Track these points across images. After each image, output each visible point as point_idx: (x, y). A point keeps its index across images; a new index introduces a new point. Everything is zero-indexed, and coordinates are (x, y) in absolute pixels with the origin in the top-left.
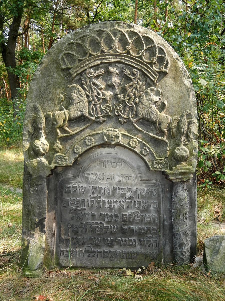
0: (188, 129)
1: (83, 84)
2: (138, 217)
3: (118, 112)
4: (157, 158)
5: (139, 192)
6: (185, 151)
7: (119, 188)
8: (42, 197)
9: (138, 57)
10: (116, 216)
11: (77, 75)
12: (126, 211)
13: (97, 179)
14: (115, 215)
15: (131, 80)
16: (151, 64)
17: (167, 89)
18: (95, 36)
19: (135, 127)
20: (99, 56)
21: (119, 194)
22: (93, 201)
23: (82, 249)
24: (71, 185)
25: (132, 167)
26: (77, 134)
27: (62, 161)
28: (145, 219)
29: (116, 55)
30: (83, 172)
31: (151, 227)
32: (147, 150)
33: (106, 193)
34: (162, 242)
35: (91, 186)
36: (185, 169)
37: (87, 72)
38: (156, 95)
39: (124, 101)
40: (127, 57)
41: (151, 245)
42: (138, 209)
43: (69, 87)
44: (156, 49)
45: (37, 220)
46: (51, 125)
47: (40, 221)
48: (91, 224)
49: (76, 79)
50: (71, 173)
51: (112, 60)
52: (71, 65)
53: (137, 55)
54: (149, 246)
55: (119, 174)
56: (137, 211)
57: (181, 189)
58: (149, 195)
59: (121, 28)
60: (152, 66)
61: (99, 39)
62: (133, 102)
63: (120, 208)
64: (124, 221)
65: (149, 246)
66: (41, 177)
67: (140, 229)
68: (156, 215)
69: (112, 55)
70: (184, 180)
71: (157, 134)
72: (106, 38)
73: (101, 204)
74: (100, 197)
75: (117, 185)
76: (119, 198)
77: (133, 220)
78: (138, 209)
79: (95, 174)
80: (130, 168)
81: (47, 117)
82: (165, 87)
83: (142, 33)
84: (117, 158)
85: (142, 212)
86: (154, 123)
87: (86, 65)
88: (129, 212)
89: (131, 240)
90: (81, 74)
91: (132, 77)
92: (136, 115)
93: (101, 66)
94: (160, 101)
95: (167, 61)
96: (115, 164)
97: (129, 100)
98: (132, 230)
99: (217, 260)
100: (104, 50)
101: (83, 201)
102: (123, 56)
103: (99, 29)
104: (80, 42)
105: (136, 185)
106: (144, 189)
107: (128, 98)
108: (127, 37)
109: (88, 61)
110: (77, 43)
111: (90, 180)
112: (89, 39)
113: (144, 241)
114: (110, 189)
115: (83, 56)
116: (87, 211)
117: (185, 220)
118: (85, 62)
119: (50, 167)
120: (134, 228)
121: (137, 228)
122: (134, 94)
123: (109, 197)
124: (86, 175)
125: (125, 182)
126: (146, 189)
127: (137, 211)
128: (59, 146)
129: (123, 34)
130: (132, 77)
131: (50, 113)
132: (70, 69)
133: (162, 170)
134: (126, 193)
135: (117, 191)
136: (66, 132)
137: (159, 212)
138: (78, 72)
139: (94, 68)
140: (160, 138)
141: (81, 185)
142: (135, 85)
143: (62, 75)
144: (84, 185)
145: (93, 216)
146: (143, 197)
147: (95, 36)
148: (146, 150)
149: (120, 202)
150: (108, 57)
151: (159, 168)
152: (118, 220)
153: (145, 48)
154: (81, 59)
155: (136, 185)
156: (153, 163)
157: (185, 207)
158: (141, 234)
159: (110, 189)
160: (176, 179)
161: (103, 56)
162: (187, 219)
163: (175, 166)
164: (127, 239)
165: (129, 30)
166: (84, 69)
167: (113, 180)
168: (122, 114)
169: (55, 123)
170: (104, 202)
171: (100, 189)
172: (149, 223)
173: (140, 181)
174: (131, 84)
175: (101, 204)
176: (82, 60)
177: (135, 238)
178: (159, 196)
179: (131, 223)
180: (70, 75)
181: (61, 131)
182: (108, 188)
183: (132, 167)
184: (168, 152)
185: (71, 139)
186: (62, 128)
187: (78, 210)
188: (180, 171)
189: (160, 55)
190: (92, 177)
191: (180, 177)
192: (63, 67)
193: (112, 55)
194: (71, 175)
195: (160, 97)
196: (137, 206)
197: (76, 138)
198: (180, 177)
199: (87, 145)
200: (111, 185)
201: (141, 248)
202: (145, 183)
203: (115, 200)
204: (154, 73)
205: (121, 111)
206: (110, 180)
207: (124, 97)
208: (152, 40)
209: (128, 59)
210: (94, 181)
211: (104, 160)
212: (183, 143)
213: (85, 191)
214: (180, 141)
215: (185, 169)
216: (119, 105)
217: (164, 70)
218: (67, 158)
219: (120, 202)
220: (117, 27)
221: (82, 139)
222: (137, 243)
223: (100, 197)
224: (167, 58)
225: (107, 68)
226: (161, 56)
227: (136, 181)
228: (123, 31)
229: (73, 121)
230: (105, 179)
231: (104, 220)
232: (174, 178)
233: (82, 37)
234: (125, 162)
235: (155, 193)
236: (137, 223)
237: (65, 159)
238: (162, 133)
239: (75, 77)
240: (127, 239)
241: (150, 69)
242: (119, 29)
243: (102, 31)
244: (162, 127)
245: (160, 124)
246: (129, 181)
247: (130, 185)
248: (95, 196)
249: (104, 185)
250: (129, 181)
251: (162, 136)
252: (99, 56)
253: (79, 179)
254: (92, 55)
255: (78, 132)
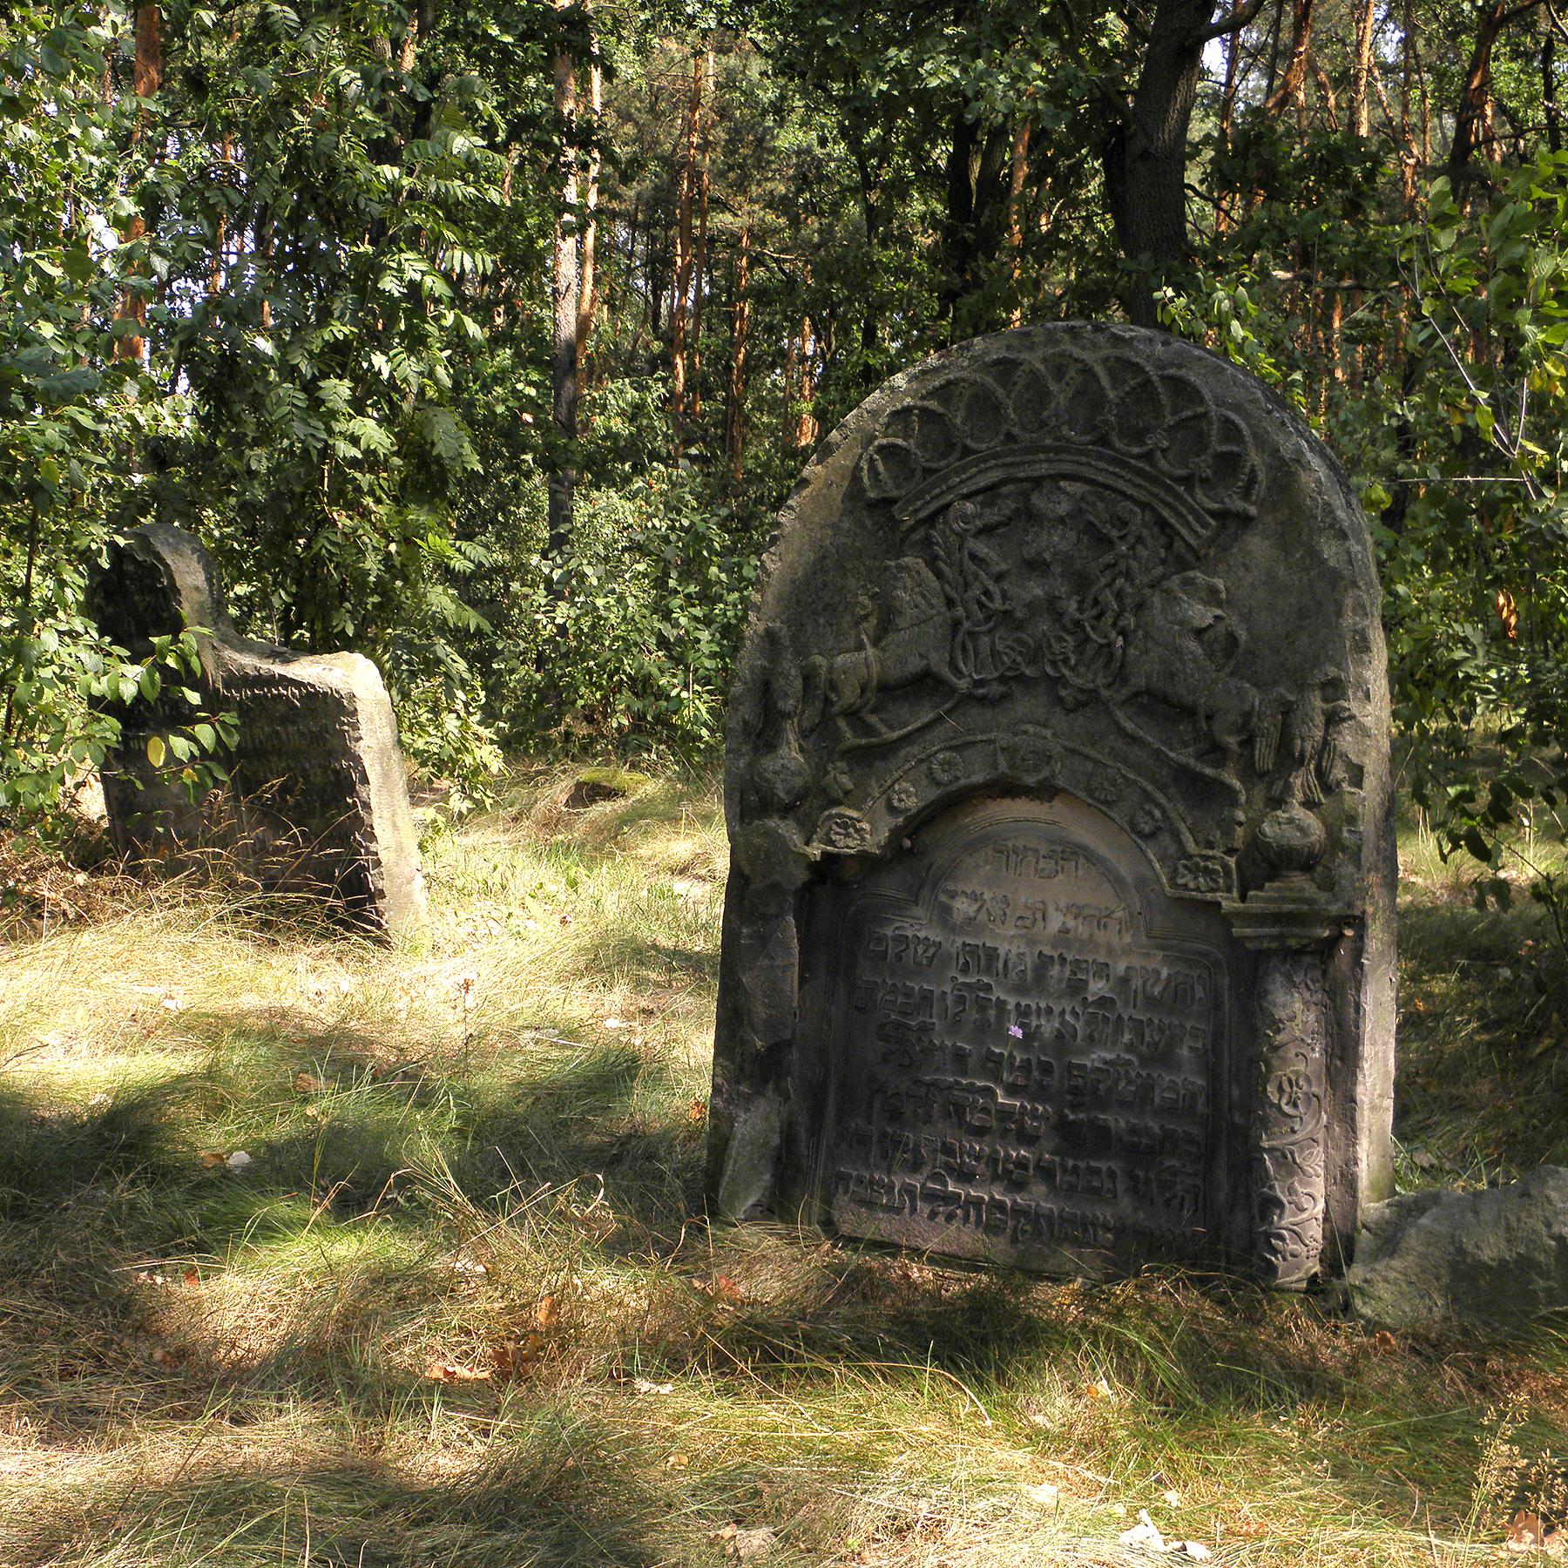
0: (1325, 742)
1: (936, 557)
2: (1129, 1083)
3: (1054, 664)
4: (1191, 846)
5: (1136, 983)
6: (1301, 829)
7: (1063, 959)
8: (779, 962)
9: (1138, 457)
10: (1046, 1069)
11: (920, 523)
12: (1083, 1052)
13: (983, 916)
14: (1039, 1062)
15: (1111, 544)
16: (1187, 481)
17: (1249, 579)
18: (989, 380)
19: (1117, 724)
20: (997, 456)
21: (1060, 980)
22: (961, 1000)
23: (916, 1181)
24: (889, 932)
25: (1117, 881)
26: (907, 739)
27: (847, 835)
28: (1157, 1091)
29: (1057, 450)
30: (935, 884)
31: (1178, 1127)
32: (1157, 814)
33: (1013, 975)
34: (1222, 1196)
35: (959, 943)
36: (1294, 901)
37: (951, 513)
38: (1206, 603)
39: (1078, 623)
40: (1100, 457)
41: (1176, 1202)
42: (1130, 1048)
43: (887, 569)
44: (1210, 423)
45: (759, 1044)
46: (819, 704)
47: (770, 1049)
48: (950, 1087)
49: (916, 537)
50: (890, 886)
51: (1043, 469)
52: (898, 487)
53: (1136, 450)
54: (1168, 1202)
55: (1062, 904)
56: (1127, 1057)
57: (1279, 978)
58: (1176, 996)
59: (1083, 348)
60: (1190, 490)
61: (1000, 392)
62: (1114, 625)
63: (1060, 1036)
64: (1075, 1091)
65: (1168, 1202)
66: (775, 887)
67: (1133, 1130)
68: (1200, 1082)
69: (1046, 449)
70: (1293, 943)
71: (1199, 757)
72: (1028, 386)
73: (992, 1012)
74: (988, 988)
75: (1054, 947)
76: (1060, 997)
77: (1110, 1090)
78: (1130, 1048)
79: (975, 897)
80: (1106, 886)
81: (808, 677)
82: (1241, 572)
83: (1160, 366)
84: (1061, 842)
85: (1145, 1061)
86: (1189, 712)
87: (950, 489)
88: (1096, 1057)
89: (1098, 1172)
90: (931, 520)
91: (1115, 533)
92: (1120, 676)
93: (1005, 490)
94: (1221, 628)
95: (1253, 470)
96: (1051, 865)
97: (1098, 617)
98: (1104, 1131)
99: (1386, 1280)
100: (1016, 431)
101: (927, 997)
102: (1081, 453)
103: (1003, 354)
104: (933, 404)
105: (1127, 951)
106: (1158, 973)
107: (1094, 612)
108: (1105, 381)
109: (957, 472)
110: (924, 410)
111: (958, 917)
112: (967, 394)
113: (1148, 1181)
114: (1029, 960)
115: (944, 456)
116: (942, 1038)
117: (1286, 1109)
118: (945, 478)
119: (805, 856)
120: (1112, 1124)
121: (1122, 1124)
122: (1119, 596)
123: (1021, 989)
124: (943, 898)
125: (1086, 936)
126: (1164, 973)
127: (1127, 1057)
128: (844, 779)
129: (1087, 371)
130: (1115, 533)
131: (818, 659)
132: (894, 501)
133: (1209, 896)
134: (1086, 982)
135: (1055, 971)
136: (869, 730)
137: (1212, 1071)
138: (922, 515)
139: (980, 498)
140: (1208, 771)
141: (922, 935)
142: (1122, 566)
143: (868, 523)
144: (935, 935)
145: (960, 1057)
146: (1151, 1003)
147: (989, 380)
148: (1150, 814)
149: (1063, 1013)
150: (1029, 458)
151: (1198, 889)
152: (1054, 1082)
153: (1170, 420)
154: (934, 465)
155: (1127, 951)
156: (1175, 870)
157: (1291, 1054)
158: (1139, 1152)
159: (1029, 960)
160: (1259, 938)
161: (1013, 452)
162: (1295, 1106)
163: (1261, 888)
164: (1082, 1165)
165: (1116, 352)
166: (942, 502)
167: (1040, 924)
168: (1066, 672)
169: (833, 697)
170: (1001, 1005)
171: (992, 954)
172: (1169, 1110)
173: (1144, 940)
174: (1109, 558)
175: (992, 1012)
176: (936, 471)
177: (1115, 1165)
178: (1217, 1006)
179: (1102, 1103)
180: (894, 523)
181: (853, 728)
182: (1021, 955)
183: (1117, 881)
184: (1240, 831)
185: (884, 758)
186: (852, 714)
187: (908, 1027)
188: (1273, 908)
189: (1224, 448)
190: (963, 907)
191: (1275, 931)
192: (872, 495)
193: (1046, 449)
194: (891, 893)
195: (1219, 612)
196: (1127, 1037)
197: (902, 753)
198: (1275, 931)
199: (939, 784)
200: (1031, 942)
201: (1135, 1210)
202: (1161, 948)
203: (1043, 1005)
204: (1198, 518)
205: (1066, 661)
206: (1028, 923)
207: (1080, 610)
208: (1196, 390)
209: (1102, 465)
210: (970, 921)
211: (1010, 844)
212: (1300, 796)
213: (937, 958)
214: (1288, 788)
215: (1294, 901)
216: (1060, 639)
217: (1238, 504)
218: (866, 826)
219: (1063, 1013)
220: (1067, 346)
221: (921, 761)
222: (1120, 1188)
223: (988, 988)
224: (1255, 458)
225: (1026, 496)
226: (1231, 453)
227: (1127, 939)
228: (1090, 362)
229: (891, 691)
230: (1011, 920)
231: (997, 1079)
232: (1248, 931)
233: (942, 387)
234: (1091, 857)
235: (1199, 993)
236: (1124, 1105)
237: (857, 831)
238: (1215, 752)
239: (913, 529)
240: (1082, 1165)
241: (1184, 503)
242: (1077, 352)
243: (1013, 361)
244: (1216, 727)
245: (1209, 718)
246: (1101, 937)
247: (1103, 952)
248: (972, 980)
249: (1008, 943)
250: (1101, 937)
251: (1220, 764)
252: (997, 456)
253: (918, 911)
254: (975, 452)
255: (910, 734)
